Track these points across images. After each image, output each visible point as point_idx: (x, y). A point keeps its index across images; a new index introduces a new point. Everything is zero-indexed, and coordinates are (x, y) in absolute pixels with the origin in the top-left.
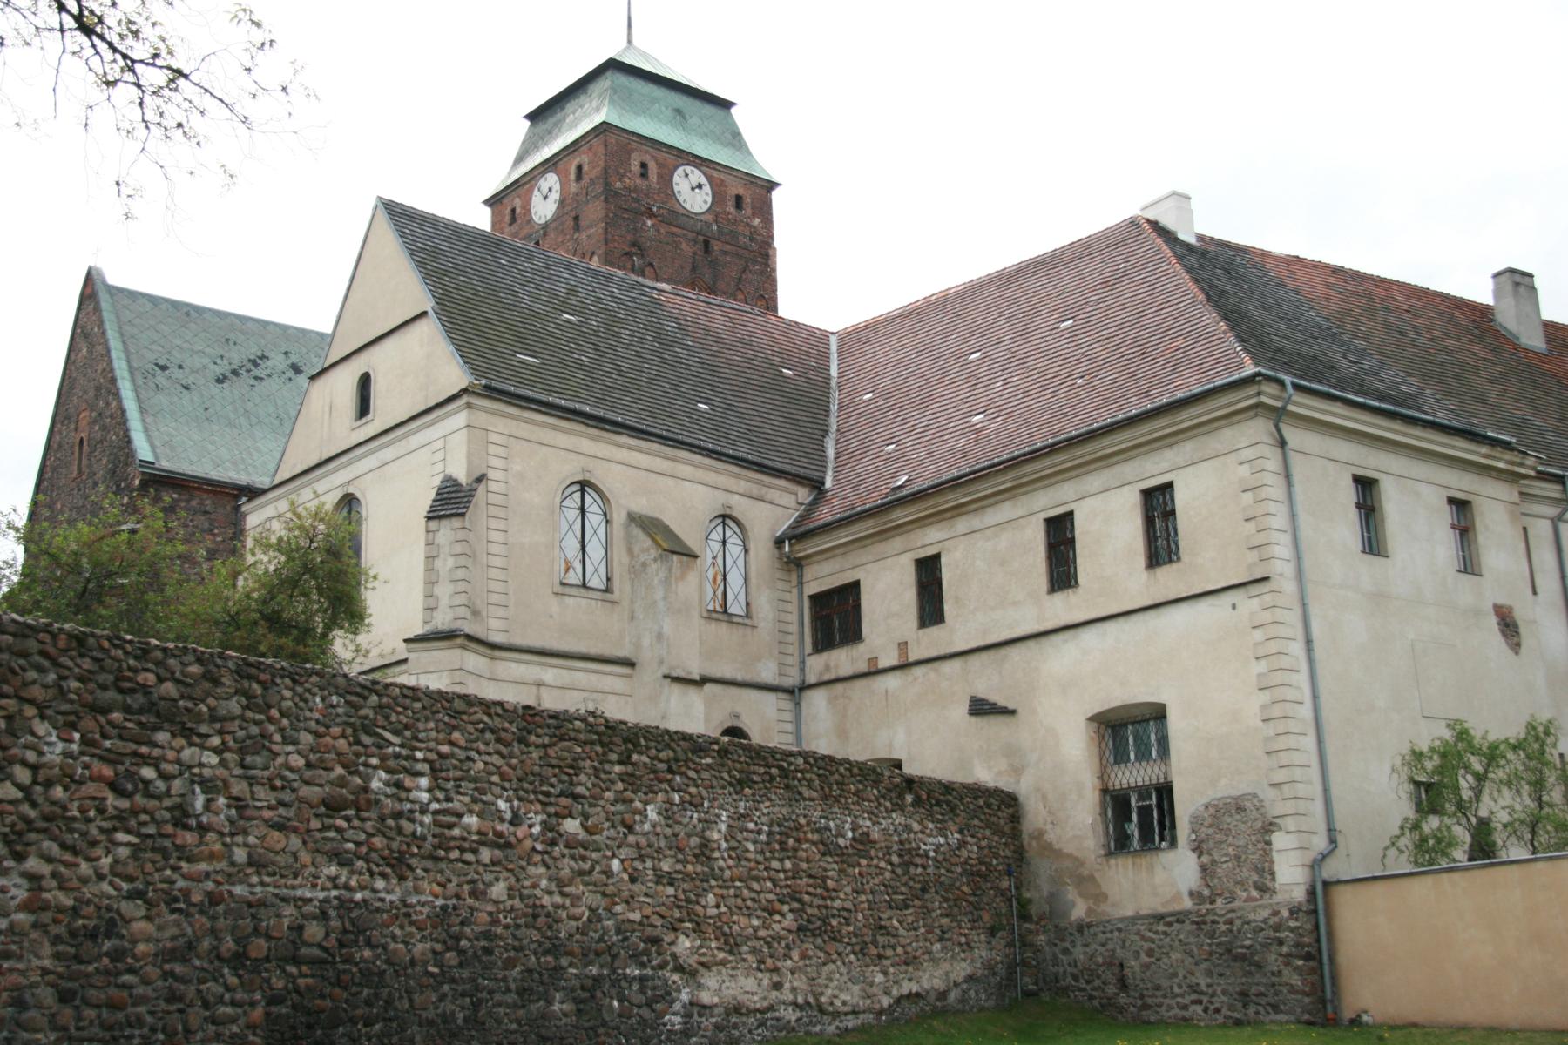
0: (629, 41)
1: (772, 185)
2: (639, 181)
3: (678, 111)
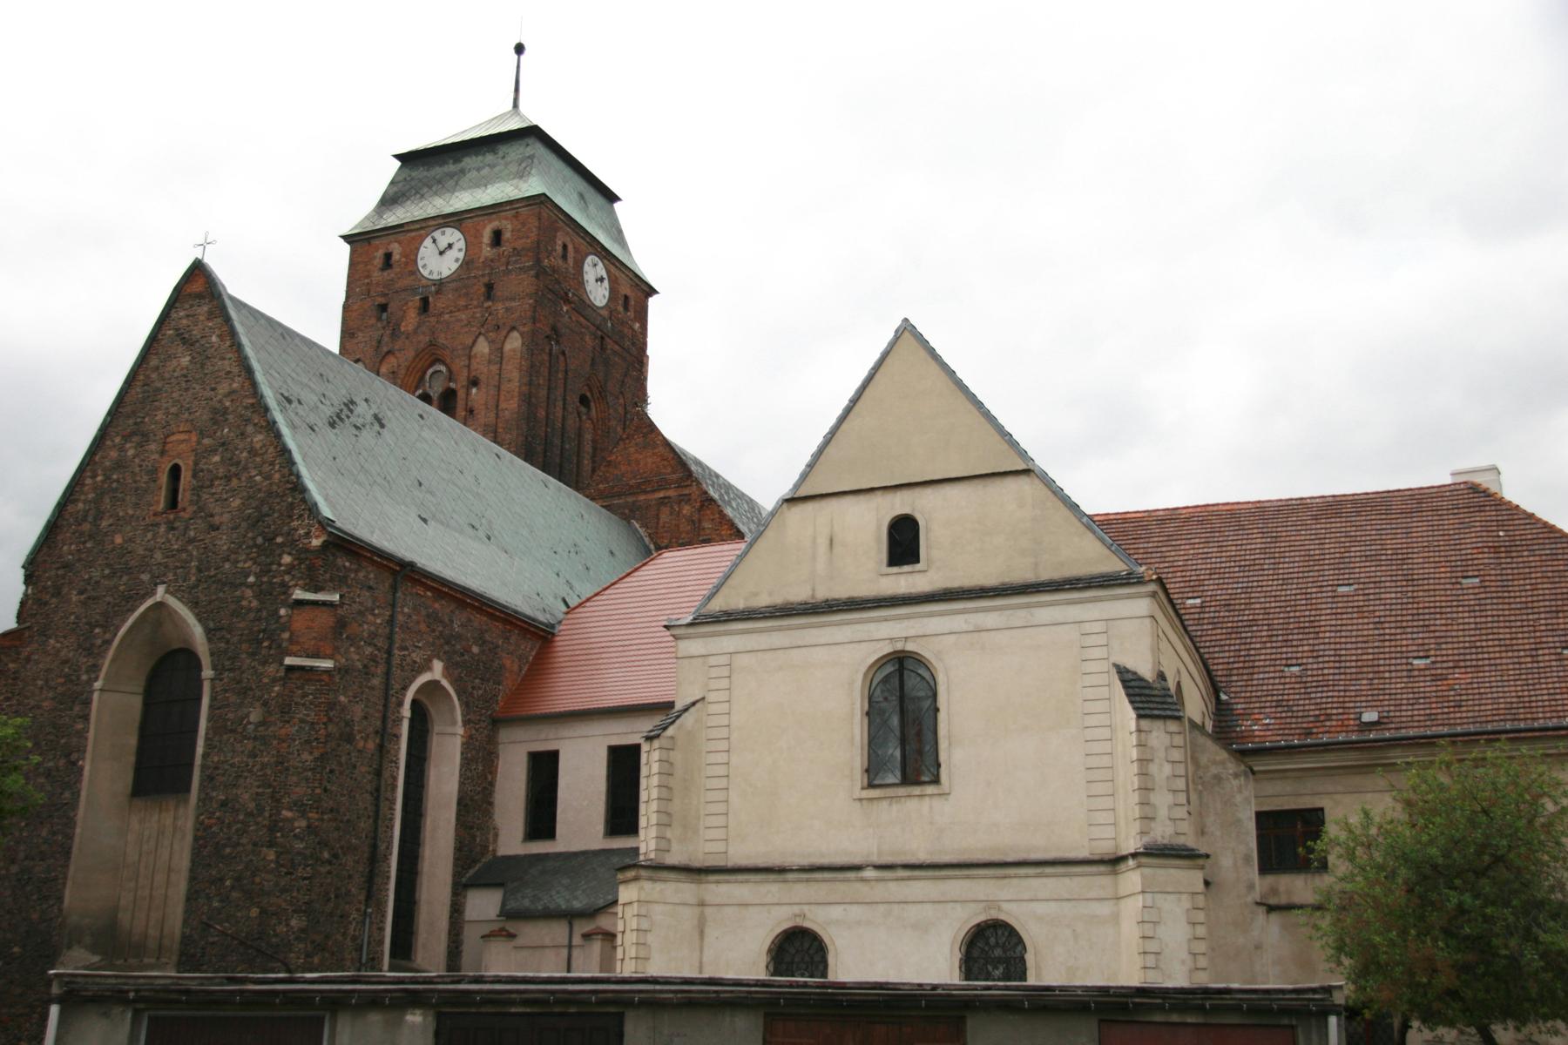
0: (516, 105)
1: (652, 291)
2: (560, 262)
3: (581, 196)
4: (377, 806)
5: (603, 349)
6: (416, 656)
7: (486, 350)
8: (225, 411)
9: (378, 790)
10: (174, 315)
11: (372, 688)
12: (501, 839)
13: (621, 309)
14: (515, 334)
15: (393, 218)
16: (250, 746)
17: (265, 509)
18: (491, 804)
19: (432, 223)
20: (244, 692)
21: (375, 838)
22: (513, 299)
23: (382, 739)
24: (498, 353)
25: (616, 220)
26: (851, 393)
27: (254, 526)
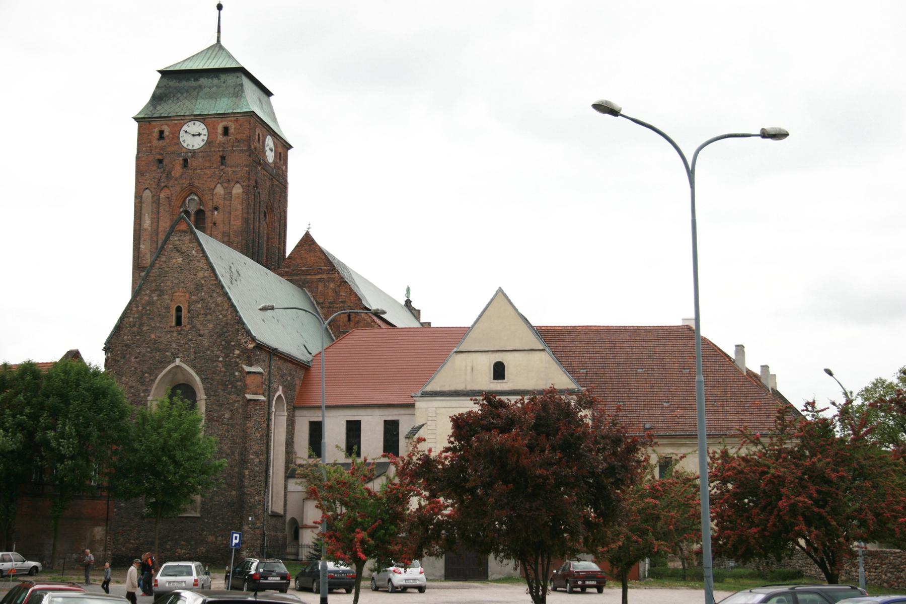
1: (291, 147)
7: (222, 192)
8: (202, 285)
10: (171, 238)
14: (238, 185)
17: (225, 330)
20: (221, 405)
24: (229, 195)
26: (479, 313)
27: (219, 336)
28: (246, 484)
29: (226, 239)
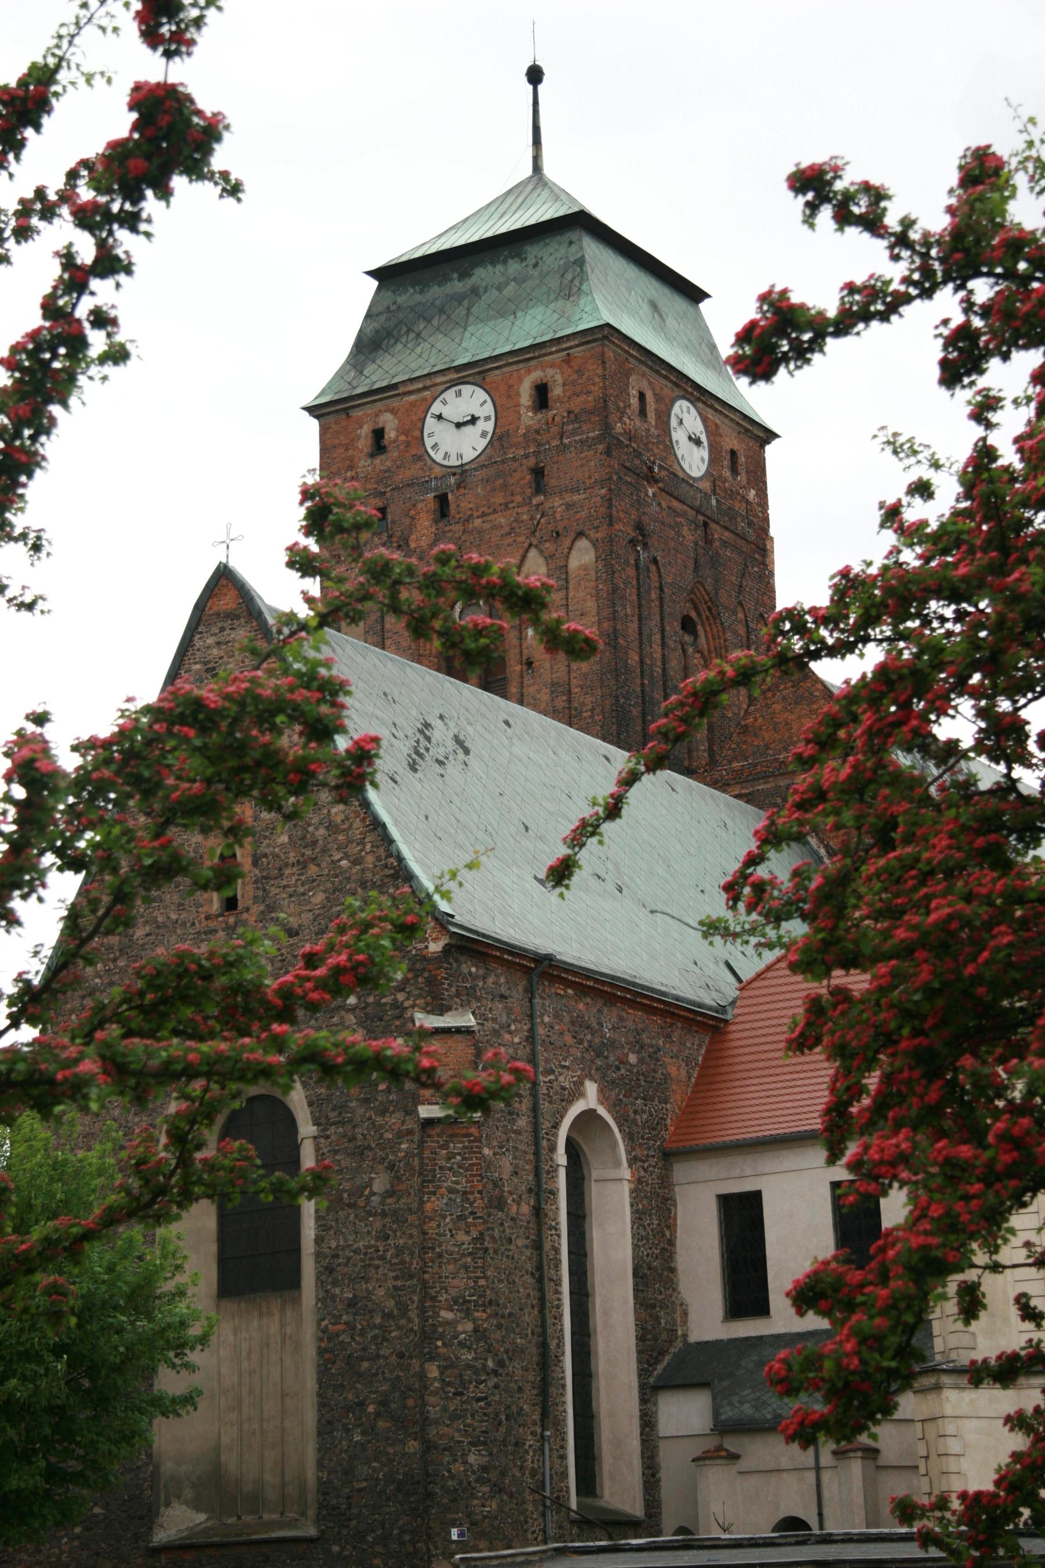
0: (537, 167)
1: (771, 435)
2: (638, 422)
3: (654, 306)
4: (541, 1290)
5: (708, 541)
6: (565, 1080)
9: (539, 1267)
10: (198, 643)
11: (518, 1132)
12: (692, 1317)
13: (727, 473)
14: (583, 543)
15: (383, 372)
16: (378, 1225)
18: (673, 1270)
19: (440, 379)
20: (360, 1153)
21: (544, 1334)
22: (575, 490)
23: (538, 1200)
25: (706, 329)
28: (434, 1412)
29: (561, 702)
